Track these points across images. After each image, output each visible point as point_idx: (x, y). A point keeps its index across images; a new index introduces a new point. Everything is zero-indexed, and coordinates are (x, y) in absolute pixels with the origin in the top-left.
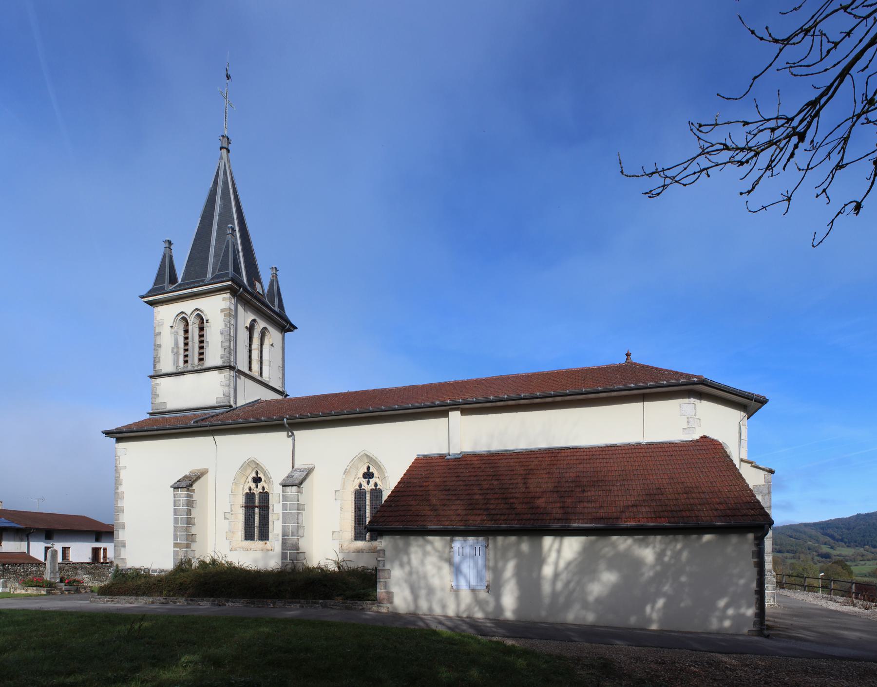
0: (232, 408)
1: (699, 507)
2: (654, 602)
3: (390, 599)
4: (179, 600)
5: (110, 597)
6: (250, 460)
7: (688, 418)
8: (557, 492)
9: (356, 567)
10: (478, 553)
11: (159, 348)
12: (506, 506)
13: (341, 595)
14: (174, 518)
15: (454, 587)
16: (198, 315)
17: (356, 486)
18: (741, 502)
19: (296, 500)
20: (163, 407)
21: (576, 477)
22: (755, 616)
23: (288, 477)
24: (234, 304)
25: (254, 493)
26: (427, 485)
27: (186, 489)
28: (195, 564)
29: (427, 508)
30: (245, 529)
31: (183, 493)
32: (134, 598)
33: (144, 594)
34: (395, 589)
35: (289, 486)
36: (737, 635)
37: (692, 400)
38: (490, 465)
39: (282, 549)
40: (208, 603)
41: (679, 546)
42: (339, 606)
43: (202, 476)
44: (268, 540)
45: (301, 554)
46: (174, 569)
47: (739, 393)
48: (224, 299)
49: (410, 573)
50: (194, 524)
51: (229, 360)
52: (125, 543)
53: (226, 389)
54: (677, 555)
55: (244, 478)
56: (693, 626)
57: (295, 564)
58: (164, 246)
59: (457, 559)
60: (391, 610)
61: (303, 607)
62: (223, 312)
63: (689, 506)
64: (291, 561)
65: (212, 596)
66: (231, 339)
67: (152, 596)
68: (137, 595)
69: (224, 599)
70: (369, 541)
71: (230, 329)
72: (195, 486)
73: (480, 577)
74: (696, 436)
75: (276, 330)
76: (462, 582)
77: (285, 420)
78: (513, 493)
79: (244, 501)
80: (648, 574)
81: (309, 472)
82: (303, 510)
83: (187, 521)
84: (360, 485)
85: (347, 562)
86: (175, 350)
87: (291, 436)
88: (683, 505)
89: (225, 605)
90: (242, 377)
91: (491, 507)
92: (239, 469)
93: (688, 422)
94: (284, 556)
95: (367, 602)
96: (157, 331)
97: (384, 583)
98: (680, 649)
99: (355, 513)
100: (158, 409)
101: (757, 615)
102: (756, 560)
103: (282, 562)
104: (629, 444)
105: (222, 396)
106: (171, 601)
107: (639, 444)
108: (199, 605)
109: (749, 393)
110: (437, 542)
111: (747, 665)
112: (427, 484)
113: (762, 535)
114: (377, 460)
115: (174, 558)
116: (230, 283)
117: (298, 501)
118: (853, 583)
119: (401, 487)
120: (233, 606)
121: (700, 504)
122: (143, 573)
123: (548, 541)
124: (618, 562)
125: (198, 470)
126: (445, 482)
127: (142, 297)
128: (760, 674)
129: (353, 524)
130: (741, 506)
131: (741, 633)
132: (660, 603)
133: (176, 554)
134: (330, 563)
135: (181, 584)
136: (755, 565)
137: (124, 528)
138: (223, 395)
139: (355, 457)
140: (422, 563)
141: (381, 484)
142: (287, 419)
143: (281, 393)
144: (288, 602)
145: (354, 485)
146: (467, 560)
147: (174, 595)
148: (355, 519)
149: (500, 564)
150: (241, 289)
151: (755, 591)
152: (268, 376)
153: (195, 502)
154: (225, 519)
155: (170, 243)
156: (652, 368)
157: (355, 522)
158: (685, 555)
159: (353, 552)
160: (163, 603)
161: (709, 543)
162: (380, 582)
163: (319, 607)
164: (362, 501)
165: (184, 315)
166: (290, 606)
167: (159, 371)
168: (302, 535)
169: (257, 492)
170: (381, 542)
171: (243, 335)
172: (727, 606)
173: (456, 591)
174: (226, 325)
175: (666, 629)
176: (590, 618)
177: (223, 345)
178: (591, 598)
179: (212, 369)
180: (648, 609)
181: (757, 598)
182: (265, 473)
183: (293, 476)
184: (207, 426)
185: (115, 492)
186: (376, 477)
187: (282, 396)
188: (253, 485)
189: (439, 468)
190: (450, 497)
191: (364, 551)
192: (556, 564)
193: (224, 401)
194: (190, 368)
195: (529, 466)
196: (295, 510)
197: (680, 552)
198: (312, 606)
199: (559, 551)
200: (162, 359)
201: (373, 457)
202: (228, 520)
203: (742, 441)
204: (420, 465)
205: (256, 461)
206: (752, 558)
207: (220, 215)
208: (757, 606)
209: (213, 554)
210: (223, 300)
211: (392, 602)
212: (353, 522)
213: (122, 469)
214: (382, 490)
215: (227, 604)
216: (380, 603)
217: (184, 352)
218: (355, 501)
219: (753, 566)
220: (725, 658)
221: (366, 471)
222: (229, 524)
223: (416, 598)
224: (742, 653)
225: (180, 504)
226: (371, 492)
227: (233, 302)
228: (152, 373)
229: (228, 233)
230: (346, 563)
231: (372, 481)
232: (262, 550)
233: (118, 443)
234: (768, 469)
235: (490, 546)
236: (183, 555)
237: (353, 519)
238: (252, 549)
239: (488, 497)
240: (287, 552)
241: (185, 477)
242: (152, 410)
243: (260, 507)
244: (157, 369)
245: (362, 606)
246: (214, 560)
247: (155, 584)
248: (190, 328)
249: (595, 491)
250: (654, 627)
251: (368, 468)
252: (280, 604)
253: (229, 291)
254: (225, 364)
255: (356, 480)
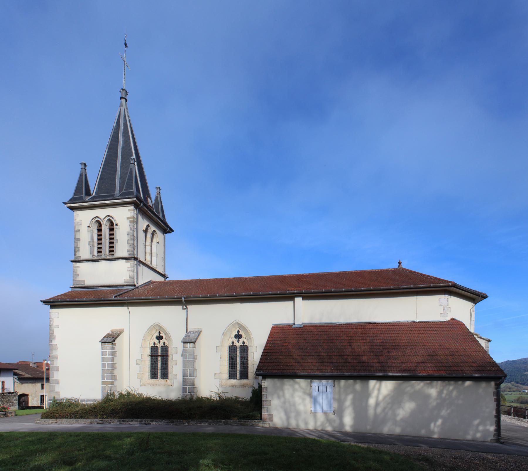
0: (136, 287)
1: (461, 365)
2: (436, 421)
3: (271, 419)
4: (113, 421)
5: (54, 420)
6: (155, 324)
7: (443, 307)
8: (373, 352)
9: (231, 397)
10: (328, 390)
11: (79, 242)
12: (343, 360)
13: (236, 416)
14: (102, 364)
15: (313, 411)
16: (109, 220)
17: (230, 343)
18: (485, 362)
19: (193, 352)
20: (82, 284)
21: (381, 342)
22: (495, 431)
23: (186, 337)
24: (136, 214)
25: (157, 347)
26: (287, 345)
27: (111, 343)
28: (117, 395)
29: (292, 360)
30: (151, 371)
31: (108, 346)
32: (75, 420)
33: (81, 417)
34: (274, 413)
35: (188, 343)
36: (484, 442)
37: (446, 296)
38: (324, 333)
39: (183, 385)
40: (137, 422)
41: (451, 388)
42: (236, 423)
43: (121, 334)
44: (168, 378)
45: (195, 389)
46: (174, 401)
47: (473, 292)
48: (129, 210)
49: (285, 403)
50: (116, 368)
51: (134, 253)
52: (59, 381)
53: (132, 274)
54: (450, 393)
55: (151, 336)
56: (458, 435)
57: (193, 395)
58: (81, 167)
59: (315, 393)
60: (271, 425)
61: (210, 424)
62: (129, 219)
63: (455, 364)
64: (190, 393)
65: (138, 418)
66: (134, 238)
67: (88, 418)
68: (75, 417)
69: (150, 420)
70: (239, 380)
71: (134, 232)
72: (116, 342)
73: (329, 404)
74: (448, 319)
75: (161, 232)
76: (318, 408)
77: (183, 298)
78: (345, 352)
79: (150, 352)
80: (433, 403)
81: (199, 333)
82: (196, 359)
83: (112, 366)
84: (233, 343)
85: (225, 393)
86: (91, 243)
87: (185, 309)
88: (451, 363)
89: (150, 424)
90: (141, 265)
91: (334, 361)
92: (147, 330)
93: (444, 310)
94: (184, 390)
95: (256, 421)
96: (77, 229)
97: (267, 409)
98: (459, 450)
99: (229, 361)
100: (78, 285)
101: (496, 430)
102: (495, 397)
103: (183, 394)
104: (408, 322)
105: (129, 278)
106: (106, 422)
107: (414, 322)
108: (129, 424)
109: (470, 289)
110: (303, 383)
111: (503, 460)
112: (286, 344)
113: (499, 383)
114: (245, 326)
115: (102, 392)
116: (135, 199)
117: (194, 353)
118: (512, 407)
119: (269, 346)
120: (157, 424)
121: (461, 363)
122: (73, 402)
123: (372, 383)
124: (414, 396)
125: (117, 330)
126: (298, 343)
127: (65, 203)
128: (512, 465)
129: (228, 369)
130: (486, 365)
131: (486, 441)
132: (439, 422)
133: (103, 389)
134: (213, 394)
135: (113, 410)
136: (494, 400)
137: (58, 370)
138: (130, 277)
139: (230, 324)
140: (292, 396)
141: (247, 342)
142: (184, 298)
143: (163, 276)
144: (199, 421)
145: (229, 343)
146: (321, 394)
147: (107, 418)
148: (229, 365)
149: (343, 397)
150: (142, 204)
151: (495, 416)
152: (155, 264)
153: (116, 352)
154: (136, 364)
155: (85, 165)
156: (418, 273)
157: (229, 367)
158: (454, 393)
159: (229, 387)
160: (99, 423)
161: (469, 386)
162: (264, 408)
163: (222, 424)
164: (235, 353)
165: (98, 219)
166: (201, 424)
167: (79, 257)
168: (196, 376)
169: (159, 345)
170: (265, 382)
171: (141, 235)
172: (478, 425)
173: (314, 414)
174: (131, 229)
175: (442, 438)
176: (398, 430)
177: (129, 242)
178: (398, 418)
179: (121, 259)
180: (432, 425)
181: (496, 420)
182: (166, 334)
183: (189, 336)
184: (125, 300)
185: (49, 344)
186: (244, 338)
187: (164, 278)
188: (157, 341)
189: (291, 334)
190: (305, 354)
191: (237, 386)
192: (377, 397)
193: (130, 281)
194: (103, 257)
195: (348, 334)
196: (192, 359)
197: (452, 392)
198: (217, 424)
199: (379, 390)
200: (81, 249)
201: (242, 324)
202: (139, 365)
203: (472, 321)
204: (277, 331)
205: (160, 325)
206: (493, 396)
207: (123, 148)
208: (496, 425)
209: (128, 388)
210: (129, 211)
211: (272, 421)
212: (228, 367)
213: (56, 328)
214: (248, 346)
215: (152, 423)
216: (264, 421)
217: (98, 245)
218: (229, 353)
219: (494, 401)
220: (489, 456)
221: (237, 333)
222: (140, 368)
223: (288, 418)
224: (497, 453)
225: (106, 354)
226: (240, 348)
227: (136, 212)
228: (73, 259)
229: (131, 162)
230: (224, 394)
231: (241, 340)
232: (165, 385)
233: (52, 309)
234: (487, 339)
235: (336, 386)
236: (109, 389)
237: (228, 365)
238: (157, 385)
239: (329, 354)
240: (187, 387)
241: (108, 334)
242: (74, 285)
243: (162, 356)
244: (77, 256)
245: (252, 423)
246: (129, 392)
247: (91, 410)
248: (103, 229)
249: (395, 352)
250: (436, 436)
251: (238, 332)
252: (193, 423)
253: (133, 205)
254: (131, 256)
255: (230, 339)
